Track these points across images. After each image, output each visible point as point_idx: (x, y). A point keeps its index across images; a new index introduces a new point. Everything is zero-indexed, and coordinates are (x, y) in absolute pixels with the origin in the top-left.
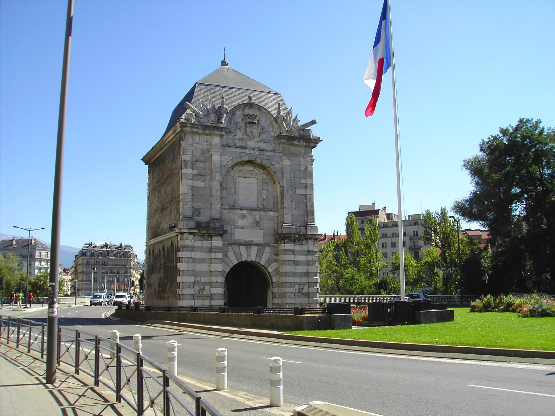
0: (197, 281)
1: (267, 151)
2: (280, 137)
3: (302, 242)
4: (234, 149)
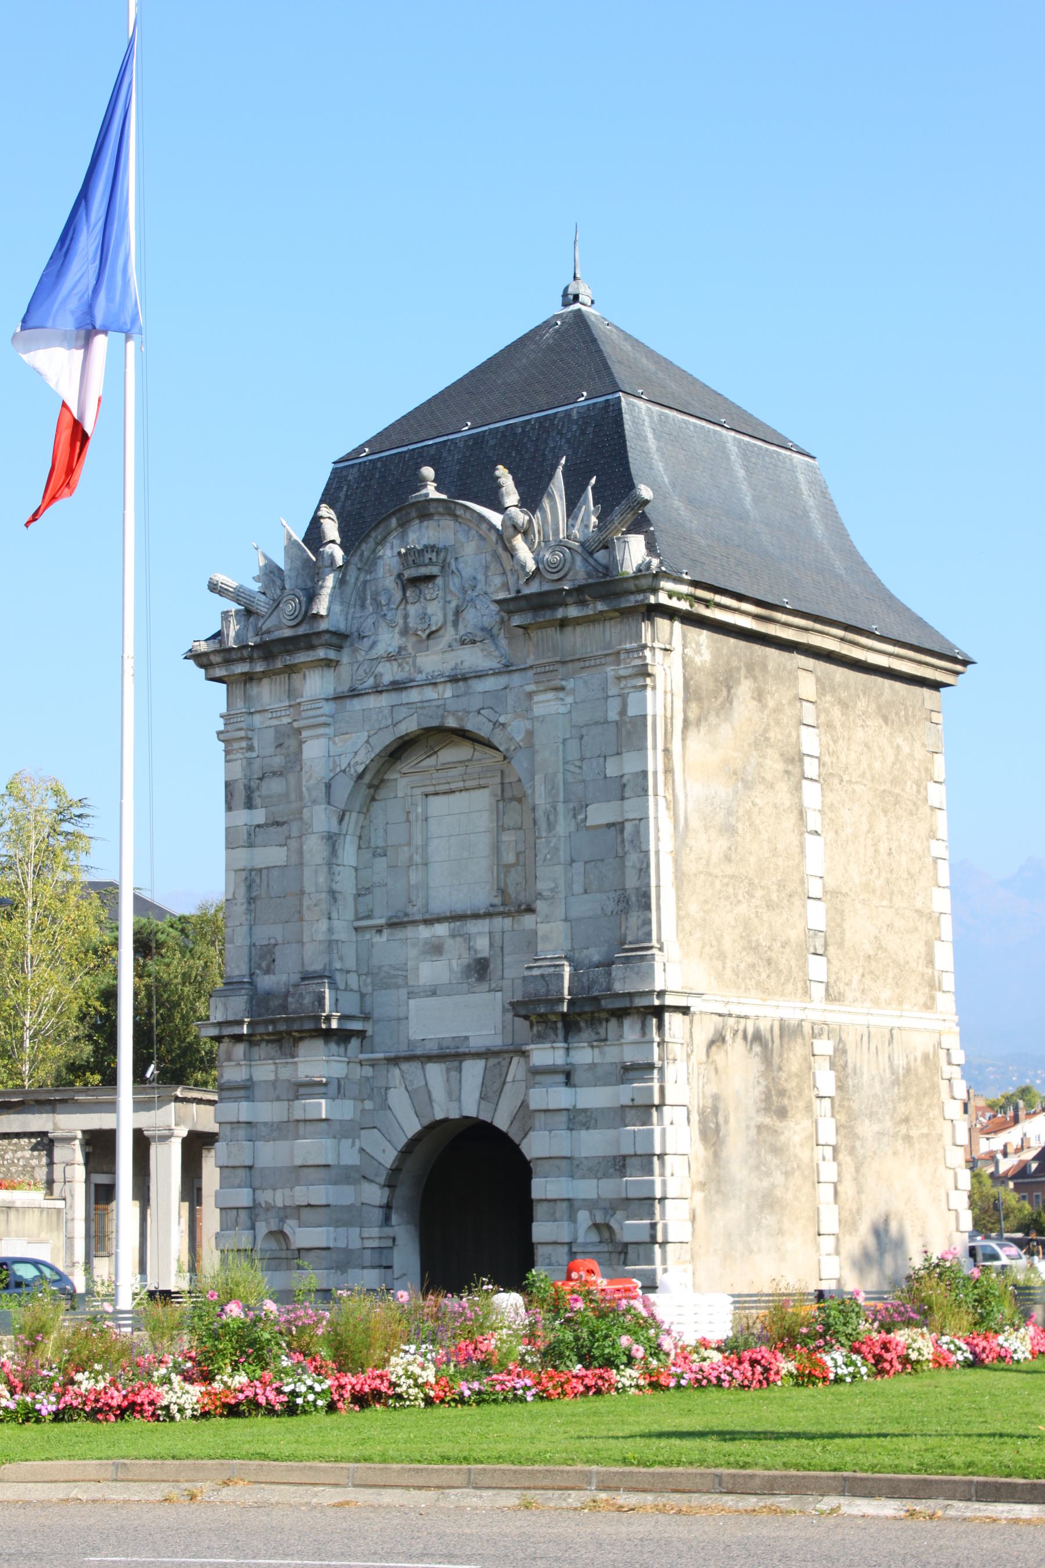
0: (263, 1205)
1: (480, 675)
2: (509, 606)
3: (602, 1031)
4: (372, 702)
